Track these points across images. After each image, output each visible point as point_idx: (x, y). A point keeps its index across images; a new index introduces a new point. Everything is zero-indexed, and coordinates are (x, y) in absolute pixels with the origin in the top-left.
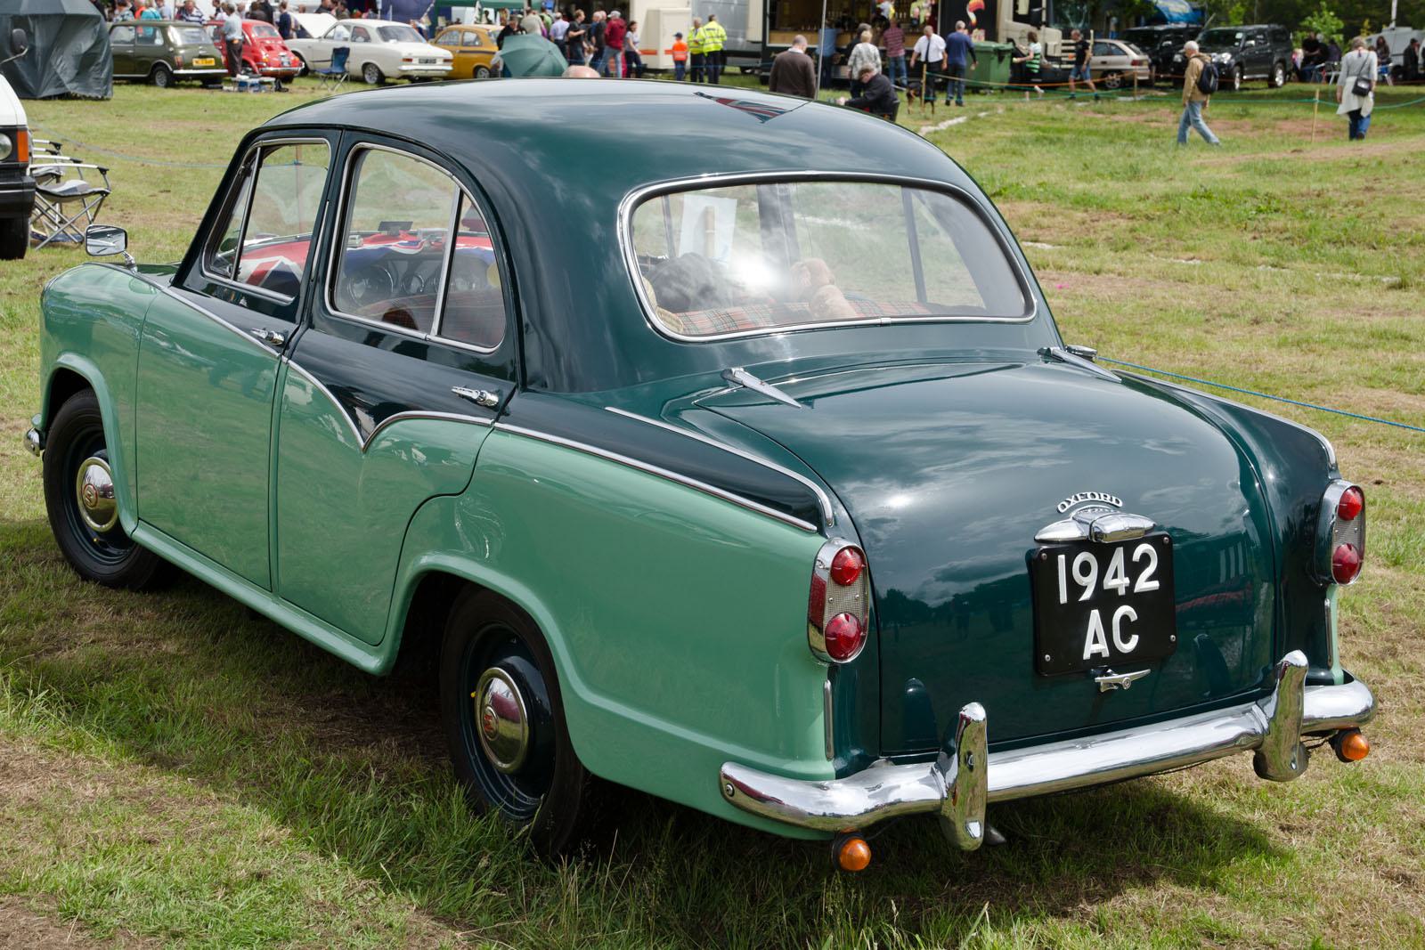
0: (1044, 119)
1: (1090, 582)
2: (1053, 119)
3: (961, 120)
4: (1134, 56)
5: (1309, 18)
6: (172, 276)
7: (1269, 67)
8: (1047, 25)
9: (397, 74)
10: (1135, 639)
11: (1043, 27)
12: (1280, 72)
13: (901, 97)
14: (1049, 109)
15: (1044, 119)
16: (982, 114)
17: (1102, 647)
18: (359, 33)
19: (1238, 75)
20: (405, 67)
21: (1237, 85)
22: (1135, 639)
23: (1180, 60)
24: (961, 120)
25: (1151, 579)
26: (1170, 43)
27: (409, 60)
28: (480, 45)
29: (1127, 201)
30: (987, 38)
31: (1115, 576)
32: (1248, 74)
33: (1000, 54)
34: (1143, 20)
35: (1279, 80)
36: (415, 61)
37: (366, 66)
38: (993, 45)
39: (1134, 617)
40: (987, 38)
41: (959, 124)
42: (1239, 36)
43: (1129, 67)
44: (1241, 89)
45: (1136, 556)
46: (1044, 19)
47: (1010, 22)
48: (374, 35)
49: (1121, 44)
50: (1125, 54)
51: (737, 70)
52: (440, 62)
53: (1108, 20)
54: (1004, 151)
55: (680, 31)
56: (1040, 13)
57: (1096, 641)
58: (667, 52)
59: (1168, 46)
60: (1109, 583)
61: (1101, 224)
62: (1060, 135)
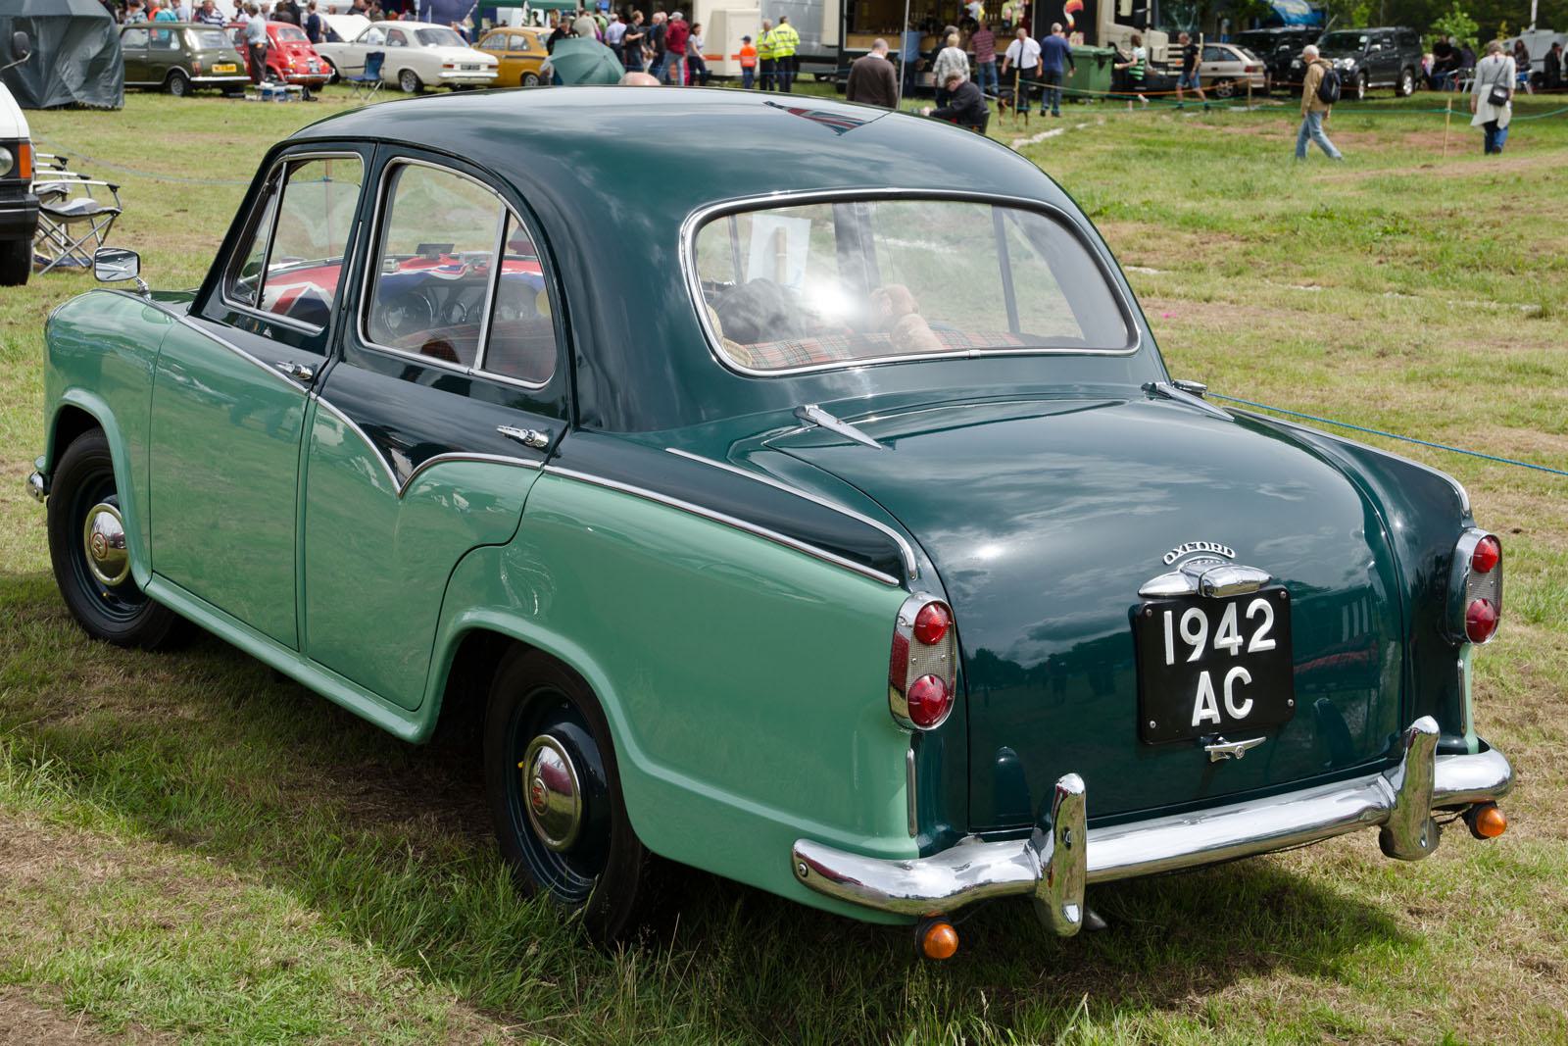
0: (1148, 131)
1: (1199, 641)
2: (1159, 131)
3: (1057, 132)
4: (1248, 62)
5: (1441, 20)
6: (189, 304)
7: (1397, 73)
8: (1152, 27)
9: (437, 81)
10: (1249, 704)
11: (1148, 30)
12: (1409, 79)
13: (992, 107)
14: (1154, 120)
15: (1148, 131)
16: (1081, 126)
17: (1213, 713)
18: (395, 37)
19: (1362, 82)
20: (446, 74)
21: (1362, 94)
22: (1249, 704)
23: (1298, 66)
24: (1057, 132)
25: (1266, 637)
26: (1287, 47)
27: (450, 66)
28: (528, 50)
29: (1240, 222)
30: (1086, 42)
31: (1227, 634)
32: (1373, 81)
33: (1100, 59)
34: (1257, 22)
35: (1407, 88)
36: (457, 67)
37: (402, 72)
38: (1093, 49)
39: (1248, 679)
40: (1086, 42)
41: (1055, 136)
42: (1363, 39)
43: (1242, 74)
44: (1365, 98)
45: (1250, 613)
46: (1149, 21)
47: (1112, 24)
48: (412, 38)
49: (1233, 49)
50: (1238, 59)
51: (811, 77)
52: (484, 68)
53: (1220, 22)
54: (1104, 166)
55: (748, 34)
56: (1144, 15)
57: (1206, 705)
58: (734, 57)
59: (1285, 51)
60: (1221, 642)
61: (1212, 247)
62: (1166, 149)
